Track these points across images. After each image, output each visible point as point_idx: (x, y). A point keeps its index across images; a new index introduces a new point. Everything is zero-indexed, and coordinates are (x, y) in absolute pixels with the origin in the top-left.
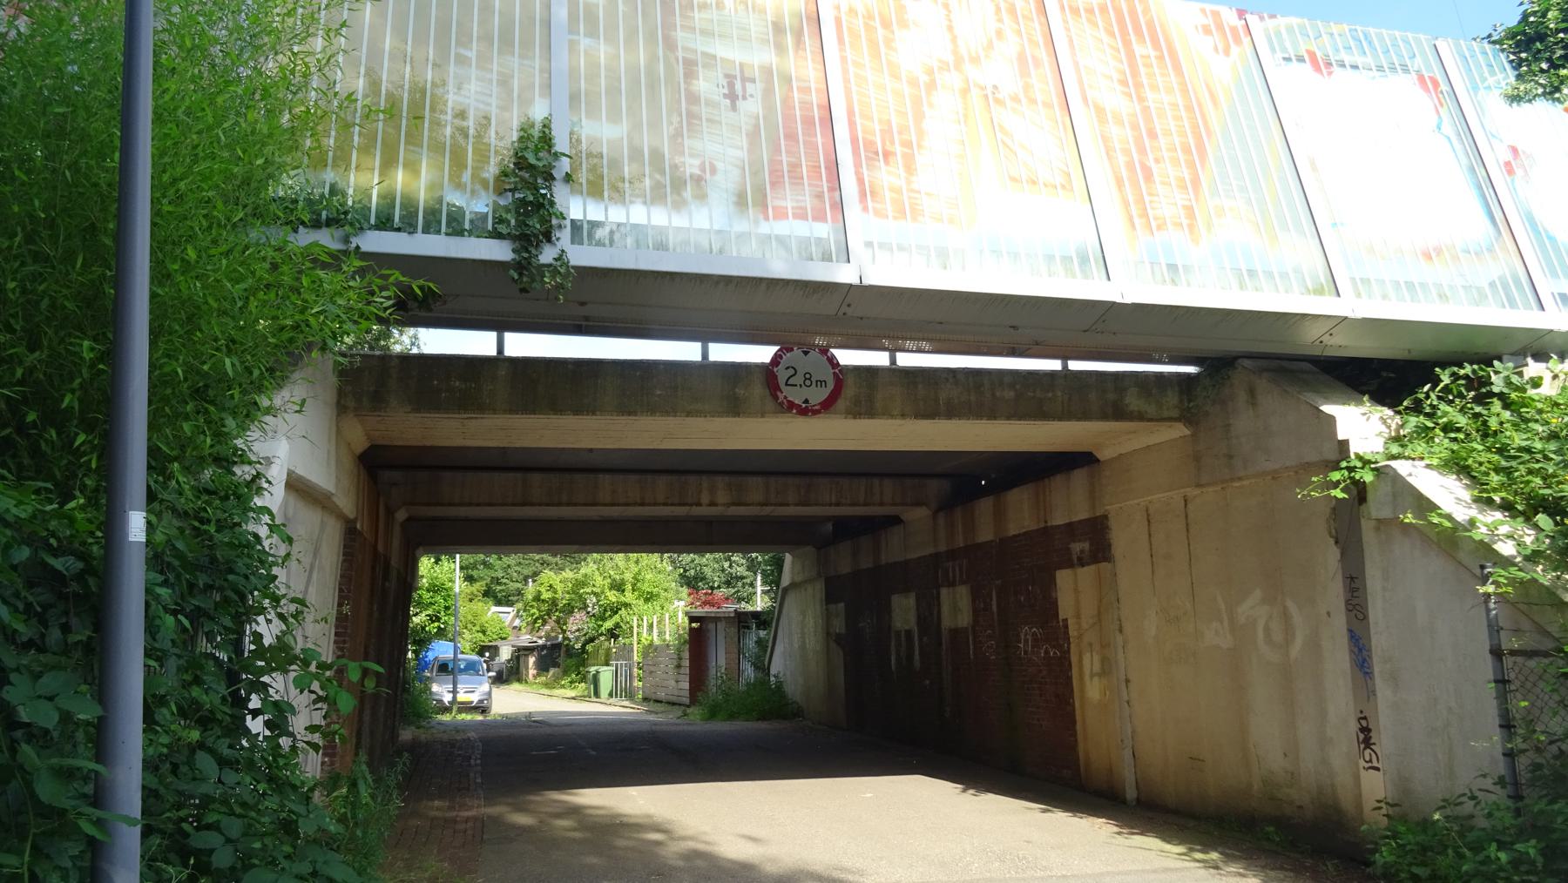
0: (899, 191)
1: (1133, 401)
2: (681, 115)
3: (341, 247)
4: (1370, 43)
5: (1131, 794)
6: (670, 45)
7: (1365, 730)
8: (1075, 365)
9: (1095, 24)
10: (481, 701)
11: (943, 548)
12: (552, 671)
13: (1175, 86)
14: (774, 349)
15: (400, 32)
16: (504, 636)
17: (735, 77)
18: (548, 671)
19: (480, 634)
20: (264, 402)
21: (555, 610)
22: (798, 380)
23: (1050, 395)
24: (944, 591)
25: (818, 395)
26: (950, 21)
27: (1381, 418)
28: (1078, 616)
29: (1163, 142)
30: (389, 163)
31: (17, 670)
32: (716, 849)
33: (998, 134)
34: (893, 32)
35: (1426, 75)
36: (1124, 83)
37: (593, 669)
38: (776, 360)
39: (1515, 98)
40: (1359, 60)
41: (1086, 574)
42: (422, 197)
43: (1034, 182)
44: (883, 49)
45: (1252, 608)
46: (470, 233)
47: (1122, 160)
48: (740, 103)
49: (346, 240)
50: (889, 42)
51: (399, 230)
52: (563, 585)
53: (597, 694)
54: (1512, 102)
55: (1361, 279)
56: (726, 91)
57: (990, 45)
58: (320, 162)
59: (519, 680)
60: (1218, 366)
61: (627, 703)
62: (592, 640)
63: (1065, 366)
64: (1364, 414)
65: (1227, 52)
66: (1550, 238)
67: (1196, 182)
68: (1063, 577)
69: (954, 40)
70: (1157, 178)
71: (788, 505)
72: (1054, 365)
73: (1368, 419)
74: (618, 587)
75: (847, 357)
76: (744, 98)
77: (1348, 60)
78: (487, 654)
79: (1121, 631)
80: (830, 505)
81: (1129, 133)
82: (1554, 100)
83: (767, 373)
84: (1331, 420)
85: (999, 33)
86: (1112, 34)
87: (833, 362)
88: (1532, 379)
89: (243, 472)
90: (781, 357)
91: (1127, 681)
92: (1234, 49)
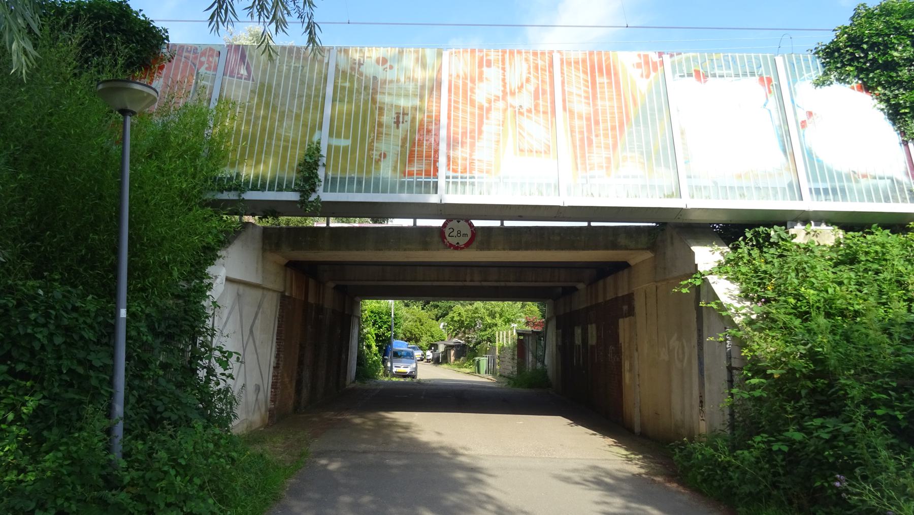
0: (465, 159)
1: (622, 240)
2: (374, 133)
3: (237, 198)
4: (735, 62)
5: (637, 429)
6: (374, 101)
7: (701, 402)
8: (593, 224)
9: (578, 69)
10: (411, 372)
11: (589, 305)
12: (462, 358)
13: (615, 97)
14: (443, 221)
16: (443, 339)
17: (400, 113)
19: (431, 338)
20: (219, 253)
21: (462, 326)
22: (455, 233)
23: (578, 238)
24: (589, 326)
25: (463, 241)
26: (504, 76)
27: (721, 252)
28: (624, 342)
29: (601, 126)
30: (258, 163)
31: (94, 351)
32: (415, 436)
33: (517, 128)
34: (475, 85)
35: (765, 76)
36: (587, 98)
37: (477, 358)
38: (445, 225)
39: (820, 83)
40: (725, 72)
41: (627, 319)
43: (531, 151)
44: (469, 93)
45: (674, 343)
46: (286, 190)
47: (578, 136)
48: (401, 125)
49: (240, 196)
50: (472, 90)
51: (259, 190)
52: (466, 313)
53: (479, 372)
54: (817, 86)
55: (696, 187)
56: (395, 120)
57: (522, 86)
58: (233, 165)
59: (447, 363)
60: (663, 226)
61: (490, 377)
62: (479, 343)
63: (589, 224)
64: (711, 251)
65: (648, 76)
66: (818, 161)
67: (615, 146)
68: (621, 321)
69: (504, 86)
70: (594, 145)
71: (510, 282)
72: (585, 224)
73: (713, 254)
74: (492, 315)
75: (477, 223)
76: (403, 122)
77: (718, 72)
78: (433, 348)
79: (637, 350)
80: (532, 281)
81: (585, 123)
82: (845, 82)
83: (441, 230)
84: (693, 254)
85: (528, 80)
86: (585, 73)
87: (471, 225)
88: (792, 235)
89: (206, 281)
90: (447, 224)
91: (639, 375)
92: (653, 74)
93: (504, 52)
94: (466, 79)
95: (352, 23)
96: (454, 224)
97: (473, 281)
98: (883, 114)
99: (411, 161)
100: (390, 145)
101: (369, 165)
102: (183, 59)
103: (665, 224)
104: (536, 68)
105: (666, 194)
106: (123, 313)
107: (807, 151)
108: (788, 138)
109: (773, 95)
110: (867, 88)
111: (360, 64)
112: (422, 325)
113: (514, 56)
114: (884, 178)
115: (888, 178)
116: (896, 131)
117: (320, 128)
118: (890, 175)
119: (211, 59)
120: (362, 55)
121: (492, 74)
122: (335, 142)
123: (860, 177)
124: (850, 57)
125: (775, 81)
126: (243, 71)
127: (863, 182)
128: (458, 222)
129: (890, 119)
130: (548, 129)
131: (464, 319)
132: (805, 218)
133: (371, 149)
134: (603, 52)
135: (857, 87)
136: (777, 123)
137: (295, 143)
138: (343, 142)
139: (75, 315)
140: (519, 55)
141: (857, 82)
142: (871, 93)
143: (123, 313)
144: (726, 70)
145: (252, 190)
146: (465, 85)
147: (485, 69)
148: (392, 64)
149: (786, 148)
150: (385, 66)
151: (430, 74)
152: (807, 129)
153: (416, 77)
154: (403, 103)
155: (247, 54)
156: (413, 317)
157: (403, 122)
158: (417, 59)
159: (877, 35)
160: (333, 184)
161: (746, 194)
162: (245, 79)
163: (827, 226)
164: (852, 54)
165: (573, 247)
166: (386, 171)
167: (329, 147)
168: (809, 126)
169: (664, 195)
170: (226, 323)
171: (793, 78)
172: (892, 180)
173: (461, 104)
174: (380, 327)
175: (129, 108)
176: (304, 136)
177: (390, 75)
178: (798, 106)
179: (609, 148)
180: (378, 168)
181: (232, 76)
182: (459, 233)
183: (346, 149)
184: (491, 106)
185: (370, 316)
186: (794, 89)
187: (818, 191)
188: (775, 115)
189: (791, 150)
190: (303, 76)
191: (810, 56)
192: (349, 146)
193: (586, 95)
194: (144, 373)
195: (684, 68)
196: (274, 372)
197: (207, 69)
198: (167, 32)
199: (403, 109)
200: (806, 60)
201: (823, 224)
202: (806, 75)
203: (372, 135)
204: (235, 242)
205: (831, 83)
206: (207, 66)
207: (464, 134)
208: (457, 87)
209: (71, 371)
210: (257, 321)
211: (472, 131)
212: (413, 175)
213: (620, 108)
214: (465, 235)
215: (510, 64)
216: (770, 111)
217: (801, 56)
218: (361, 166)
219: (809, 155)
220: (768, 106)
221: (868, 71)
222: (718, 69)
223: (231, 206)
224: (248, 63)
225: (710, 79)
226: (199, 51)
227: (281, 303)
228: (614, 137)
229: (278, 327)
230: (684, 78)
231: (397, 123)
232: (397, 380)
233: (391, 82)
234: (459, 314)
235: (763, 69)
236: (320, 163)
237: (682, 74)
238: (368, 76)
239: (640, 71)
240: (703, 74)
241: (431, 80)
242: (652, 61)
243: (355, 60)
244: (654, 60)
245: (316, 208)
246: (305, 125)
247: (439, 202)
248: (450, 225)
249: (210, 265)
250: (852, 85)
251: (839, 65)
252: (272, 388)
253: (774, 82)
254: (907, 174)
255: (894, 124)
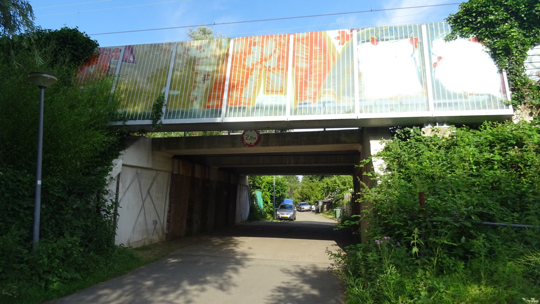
6: (193, 69)
8: (327, 129)
15: (141, 77)
17: (206, 75)
18: (329, 210)
22: (249, 138)
26: (262, 50)
30: (135, 105)
35: (414, 37)
37: (335, 209)
38: (244, 133)
39: (448, 39)
40: (389, 37)
42: (139, 112)
44: (242, 61)
48: (206, 81)
52: (331, 183)
54: (446, 41)
58: (123, 107)
63: (325, 130)
64: (380, 143)
65: (343, 44)
66: (441, 86)
67: (320, 85)
72: (322, 130)
73: (381, 144)
77: (385, 37)
78: (316, 204)
83: (242, 136)
85: (275, 52)
92: (346, 42)
93: (263, 37)
94: (242, 53)
95: (373, 11)
96: (248, 133)
97: (291, 164)
98: (488, 55)
99: (209, 101)
100: (199, 92)
101: (188, 104)
102: (104, 55)
103: (363, 128)
104: (280, 44)
105: (346, 111)
106: (39, 182)
107: (435, 81)
108: (425, 74)
109: (418, 49)
110: (479, 39)
111: (188, 50)
112: (313, 190)
113: (268, 39)
114: (484, 95)
115: (486, 95)
116: (496, 64)
117: (165, 86)
118: (489, 93)
119: (117, 54)
120: (189, 45)
121: (256, 50)
122: (172, 92)
123: (468, 95)
124: (467, 22)
125: (420, 40)
126: (131, 59)
127: (470, 99)
128: (251, 131)
129: (492, 57)
130: (283, 78)
131: (330, 186)
132: (433, 121)
133: (189, 95)
134: (433, 23)
135: (473, 39)
136: (419, 65)
137: (153, 94)
138: (176, 92)
139: (18, 183)
140: (271, 38)
141: (473, 36)
142: (481, 42)
143: (39, 182)
144: (390, 36)
145: (130, 120)
146: (241, 57)
147: (252, 47)
148: (204, 49)
149: (423, 81)
150: (201, 50)
151: (224, 51)
152: (437, 68)
153: (216, 55)
154: (209, 69)
155: (134, 49)
156: (307, 186)
157: (207, 80)
158: (217, 45)
159: (481, 6)
160: (170, 115)
161: (394, 108)
162: (132, 63)
163: (447, 125)
164: (467, 19)
165: (314, 143)
166: (196, 106)
167: (169, 95)
168: (439, 66)
169: (345, 112)
170: (128, 188)
171: (431, 38)
172: (490, 95)
173: (237, 68)
174: (273, 191)
175: (42, 85)
176: (157, 91)
177: (203, 55)
178: (433, 54)
179: (316, 87)
180: (192, 105)
181: (126, 62)
182: (251, 137)
183: (177, 96)
184: (253, 68)
185: (266, 185)
186: (432, 44)
187: (439, 105)
188: (418, 60)
189: (425, 81)
190: (160, 59)
191: (444, 23)
192: (178, 95)
193: (306, 57)
194: (61, 212)
195: (365, 37)
196: (168, 214)
197: (115, 59)
198: (97, 42)
199: (208, 72)
200: (441, 25)
201: (445, 124)
202: (440, 35)
203: (191, 88)
204: (131, 146)
205: (456, 38)
206: (115, 57)
207: (238, 84)
208: (236, 59)
209: (12, 209)
210: (152, 187)
211: (242, 82)
212: (210, 108)
213: (325, 63)
214: (255, 138)
215: (266, 43)
216: (415, 58)
217: (438, 23)
218: (184, 105)
219: (437, 85)
220: (414, 56)
221: (479, 29)
222: (385, 36)
223: (119, 129)
224: (134, 55)
225: (380, 42)
226: (112, 50)
227: (171, 177)
228: (320, 80)
229: (170, 190)
230: (364, 43)
231: (204, 80)
232: (276, 221)
233: (203, 58)
234: (327, 183)
235: (413, 33)
236: (164, 104)
237: (364, 41)
238: (192, 56)
239: (339, 41)
240: (376, 39)
241: (224, 55)
242: (346, 33)
243: (186, 48)
244: (348, 34)
245: (159, 128)
246: (158, 85)
247: (221, 122)
248: (247, 133)
249: (115, 158)
250: (470, 38)
251: (460, 27)
252: (167, 223)
253: (419, 41)
254: (500, 91)
255: (495, 60)
